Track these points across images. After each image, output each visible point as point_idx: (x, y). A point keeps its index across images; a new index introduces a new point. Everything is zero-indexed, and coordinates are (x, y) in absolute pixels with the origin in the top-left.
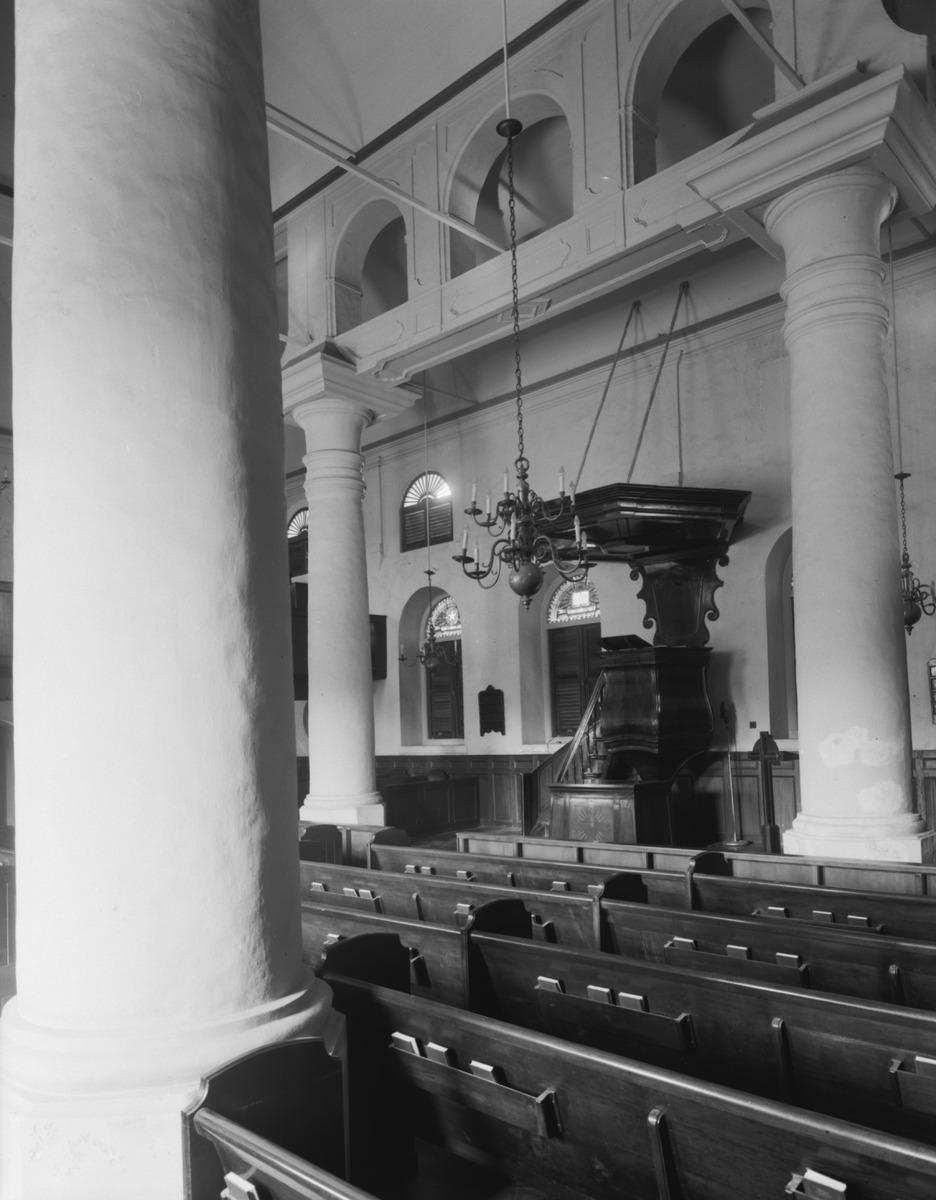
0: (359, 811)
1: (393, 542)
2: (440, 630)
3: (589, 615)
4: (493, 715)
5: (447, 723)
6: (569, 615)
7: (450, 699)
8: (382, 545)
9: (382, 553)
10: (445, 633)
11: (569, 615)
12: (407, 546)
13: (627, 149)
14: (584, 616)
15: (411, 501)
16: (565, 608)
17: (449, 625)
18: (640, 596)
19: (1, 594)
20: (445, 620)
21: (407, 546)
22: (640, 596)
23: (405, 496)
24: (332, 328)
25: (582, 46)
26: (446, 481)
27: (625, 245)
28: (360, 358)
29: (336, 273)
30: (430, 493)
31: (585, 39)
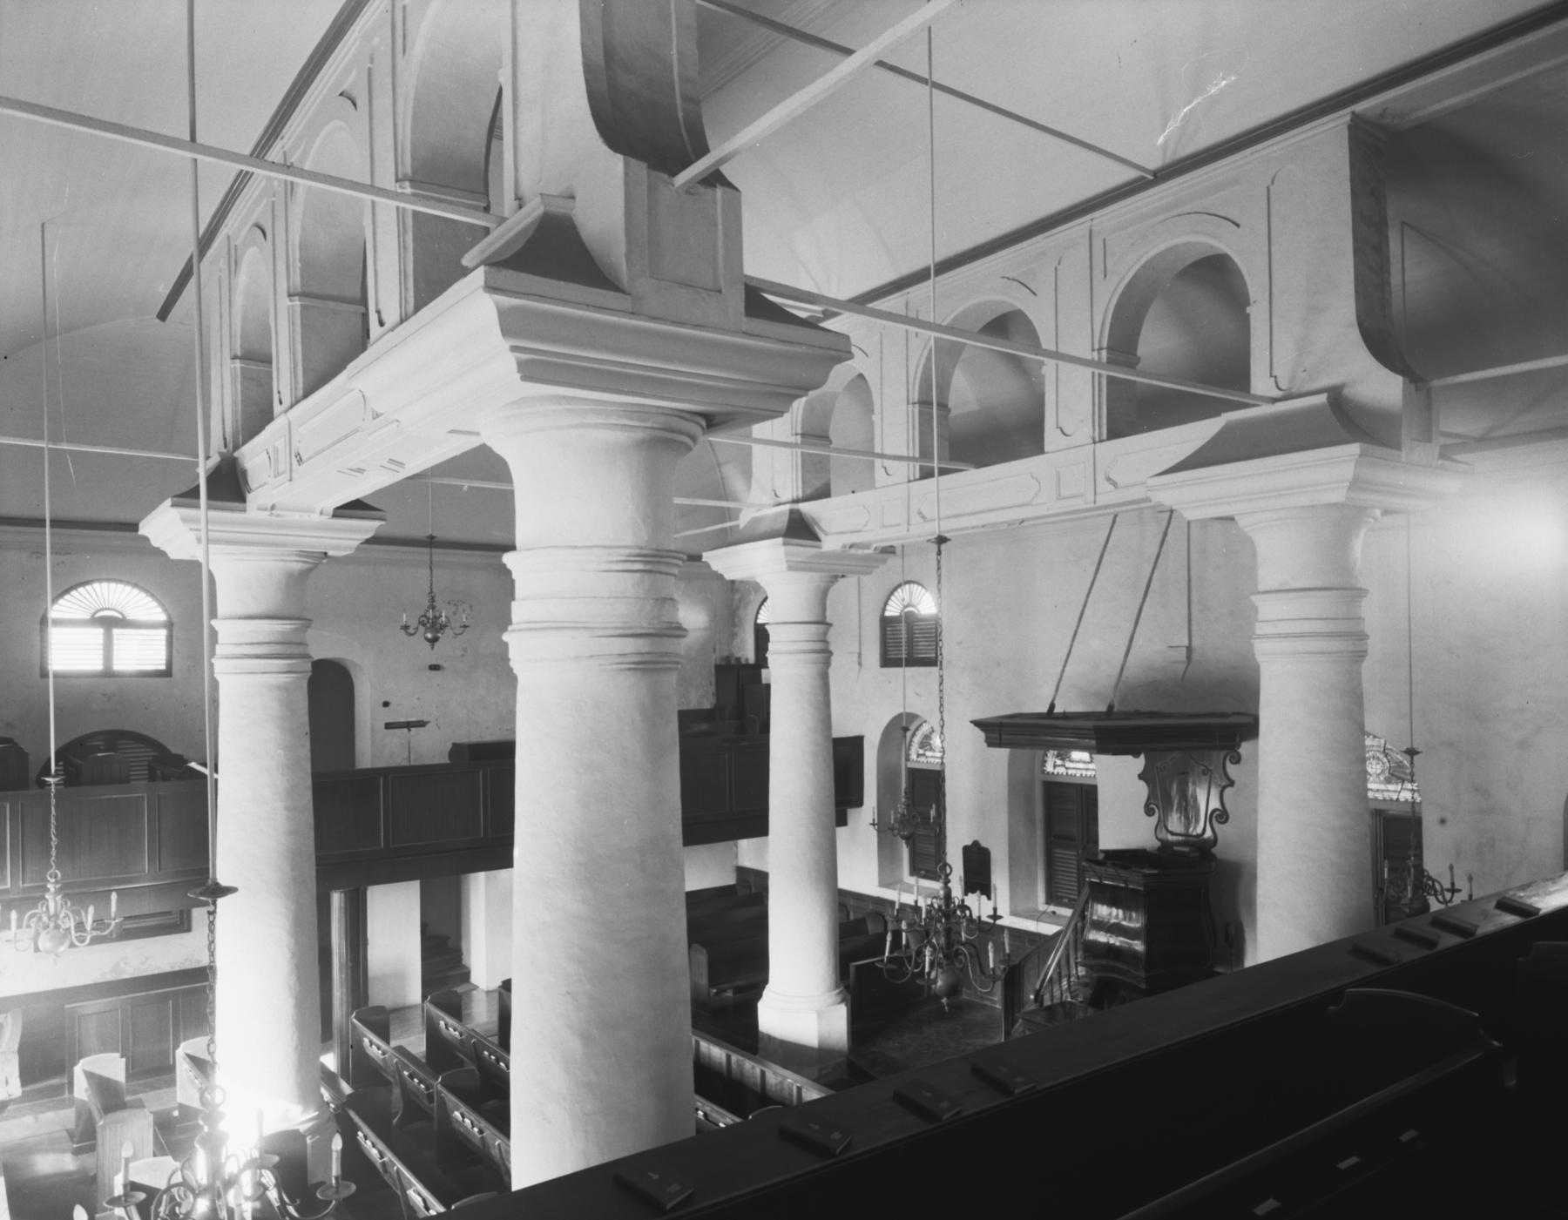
0: (820, 1015)
1: (873, 654)
2: (924, 755)
3: (1387, 795)
4: (978, 875)
5: (929, 862)
6: (1067, 768)
7: (933, 835)
8: (860, 655)
9: (860, 664)
10: (931, 760)
11: (1067, 768)
12: (887, 661)
13: (1100, 396)
14: (1084, 773)
15: (893, 610)
16: (1063, 759)
17: (934, 751)
18: (1141, 777)
19: (390, 3)
20: (930, 744)
21: (887, 661)
22: (1141, 777)
23: (886, 604)
24: (797, 490)
25: (1056, 269)
26: (926, 590)
27: (1095, 502)
28: (826, 534)
29: (802, 428)
30: (913, 606)
31: (1059, 263)
